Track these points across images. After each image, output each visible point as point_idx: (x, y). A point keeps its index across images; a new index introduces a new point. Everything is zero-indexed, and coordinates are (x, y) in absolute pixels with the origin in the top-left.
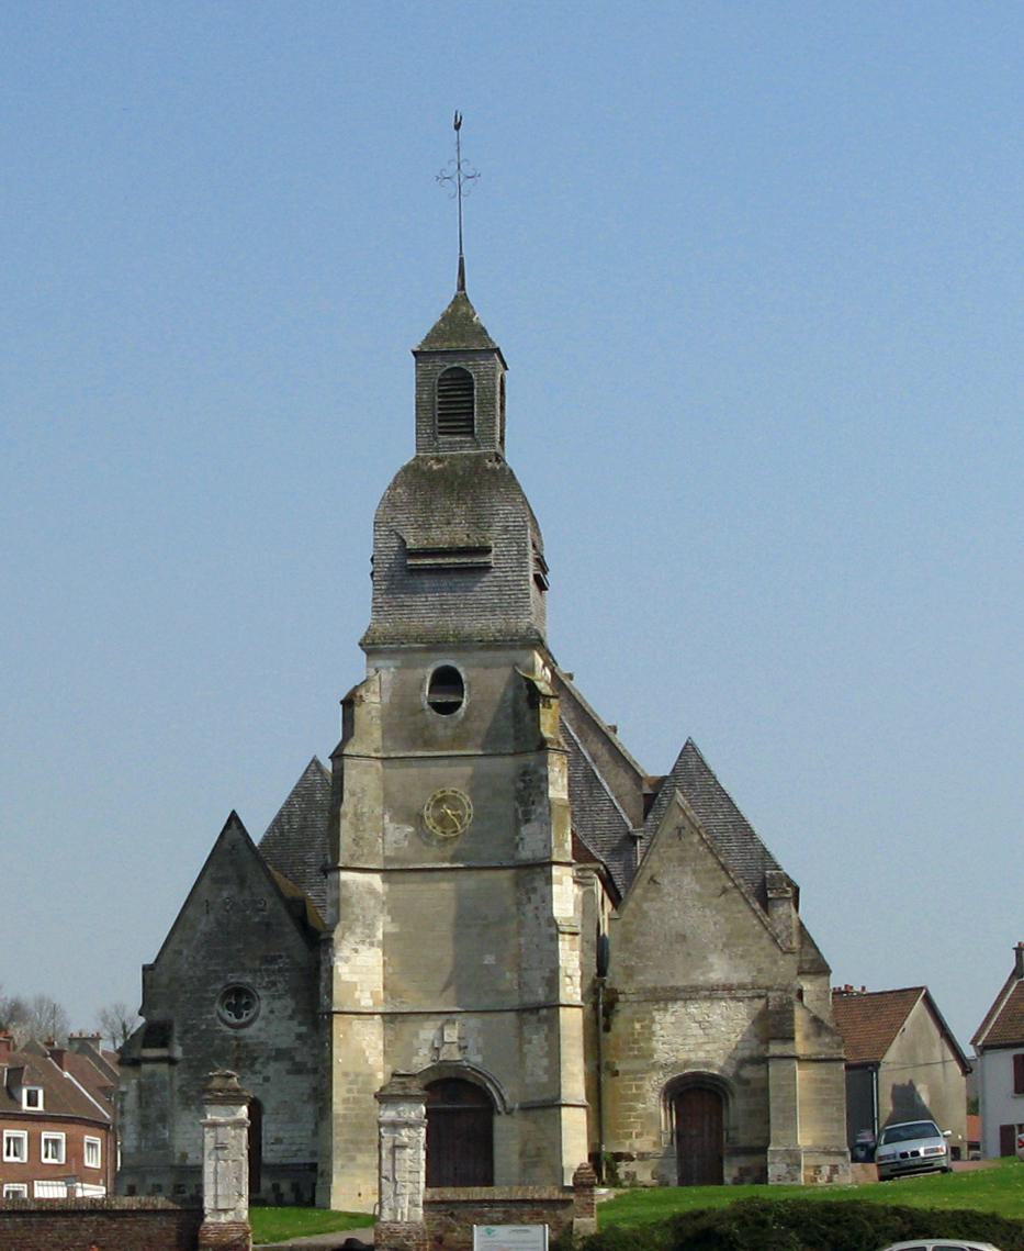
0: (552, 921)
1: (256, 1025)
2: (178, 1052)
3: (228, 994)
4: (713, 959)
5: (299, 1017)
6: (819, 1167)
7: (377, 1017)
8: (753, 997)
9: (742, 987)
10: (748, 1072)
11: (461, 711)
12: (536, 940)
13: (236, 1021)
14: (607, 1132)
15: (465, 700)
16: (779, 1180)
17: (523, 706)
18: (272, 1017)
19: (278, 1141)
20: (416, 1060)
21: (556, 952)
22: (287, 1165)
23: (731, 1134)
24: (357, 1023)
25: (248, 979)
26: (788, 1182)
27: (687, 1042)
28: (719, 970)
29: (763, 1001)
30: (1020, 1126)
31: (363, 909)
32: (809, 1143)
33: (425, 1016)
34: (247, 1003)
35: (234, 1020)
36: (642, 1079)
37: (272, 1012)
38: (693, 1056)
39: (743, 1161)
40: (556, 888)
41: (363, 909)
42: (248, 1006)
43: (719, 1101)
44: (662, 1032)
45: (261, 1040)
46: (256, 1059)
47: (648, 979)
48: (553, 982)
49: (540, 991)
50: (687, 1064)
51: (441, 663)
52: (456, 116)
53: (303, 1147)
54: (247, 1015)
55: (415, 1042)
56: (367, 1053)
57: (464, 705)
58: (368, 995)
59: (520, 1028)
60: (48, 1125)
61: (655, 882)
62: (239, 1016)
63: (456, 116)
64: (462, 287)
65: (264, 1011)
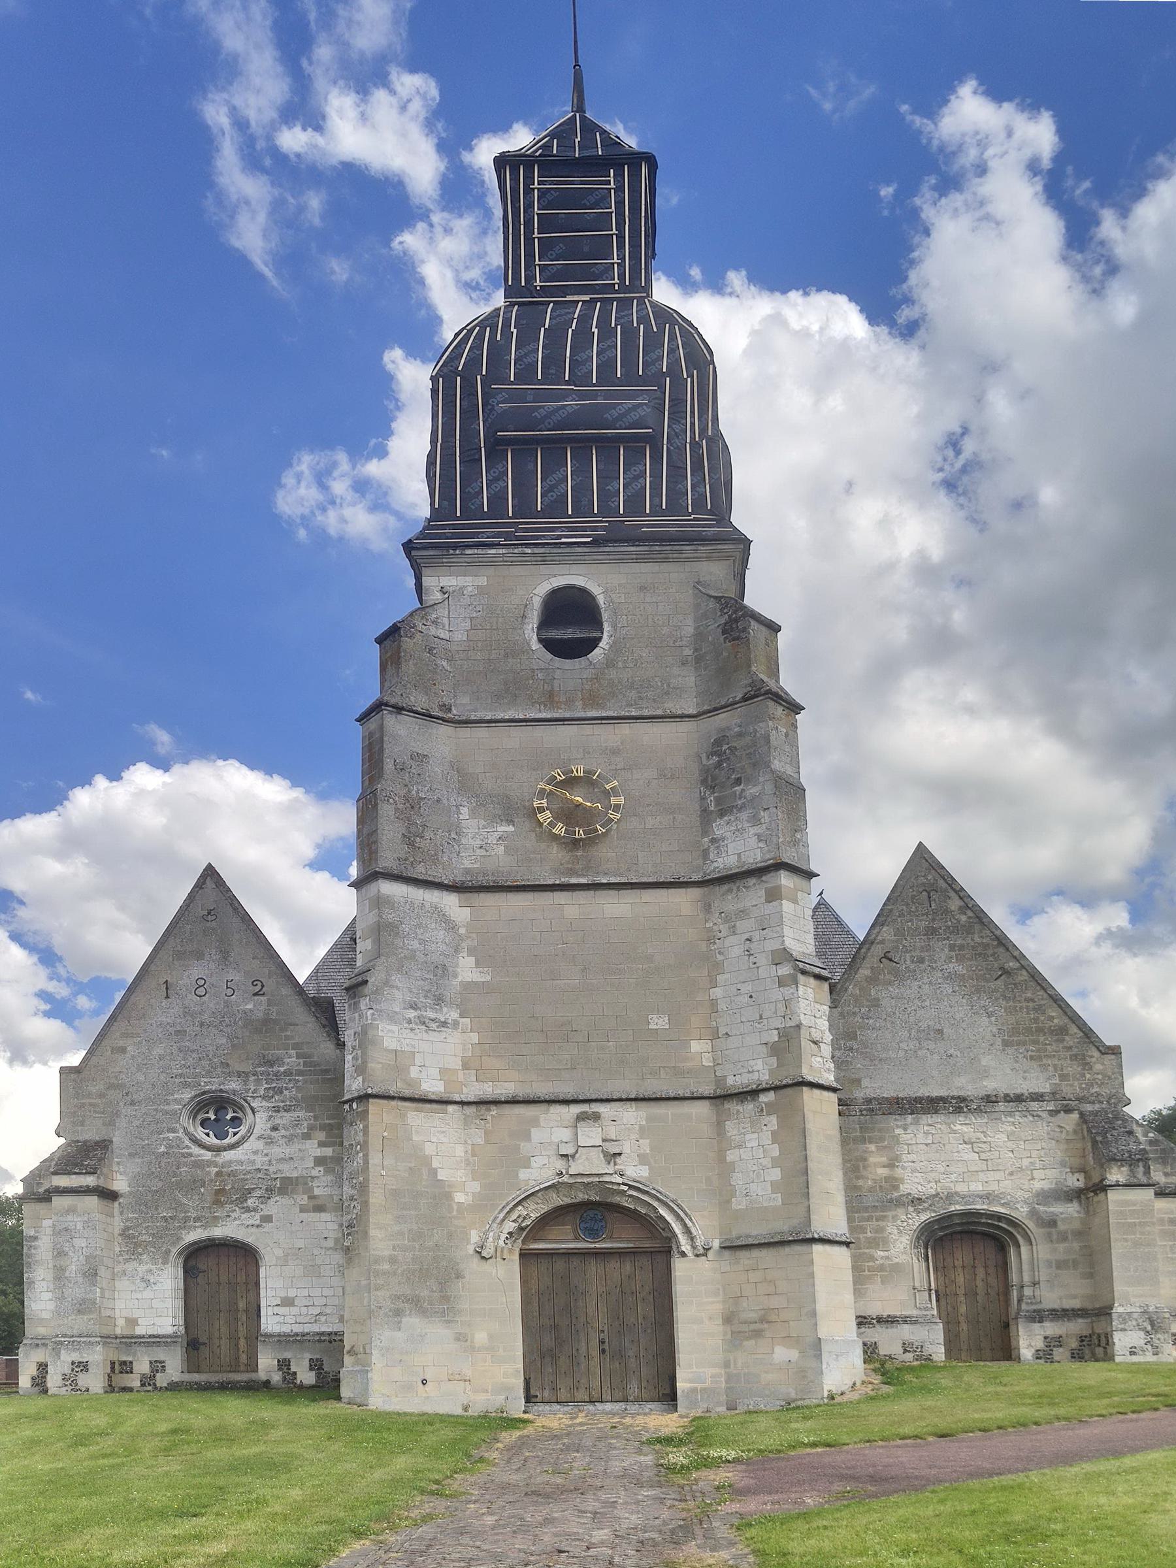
1: (252, 1144)
2: (120, 1184)
9: (1038, 1097)
11: (597, 654)
12: (747, 988)
16: (1132, 1353)
18: (274, 1134)
24: (416, 1117)
25: (233, 1085)
26: (1150, 1358)
27: (952, 1169)
31: (423, 942)
34: (233, 1119)
35: (212, 1140)
36: (883, 1218)
37: (275, 1129)
38: (961, 1188)
41: (423, 942)
42: (236, 1121)
43: (1002, 1249)
44: (912, 1157)
46: (250, 1191)
51: (580, 581)
53: (328, 1310)
54: (235, 1134)
57: (604, 643)
58: (435, 1073)
59: (720, 1126)
62: (221, 1136)
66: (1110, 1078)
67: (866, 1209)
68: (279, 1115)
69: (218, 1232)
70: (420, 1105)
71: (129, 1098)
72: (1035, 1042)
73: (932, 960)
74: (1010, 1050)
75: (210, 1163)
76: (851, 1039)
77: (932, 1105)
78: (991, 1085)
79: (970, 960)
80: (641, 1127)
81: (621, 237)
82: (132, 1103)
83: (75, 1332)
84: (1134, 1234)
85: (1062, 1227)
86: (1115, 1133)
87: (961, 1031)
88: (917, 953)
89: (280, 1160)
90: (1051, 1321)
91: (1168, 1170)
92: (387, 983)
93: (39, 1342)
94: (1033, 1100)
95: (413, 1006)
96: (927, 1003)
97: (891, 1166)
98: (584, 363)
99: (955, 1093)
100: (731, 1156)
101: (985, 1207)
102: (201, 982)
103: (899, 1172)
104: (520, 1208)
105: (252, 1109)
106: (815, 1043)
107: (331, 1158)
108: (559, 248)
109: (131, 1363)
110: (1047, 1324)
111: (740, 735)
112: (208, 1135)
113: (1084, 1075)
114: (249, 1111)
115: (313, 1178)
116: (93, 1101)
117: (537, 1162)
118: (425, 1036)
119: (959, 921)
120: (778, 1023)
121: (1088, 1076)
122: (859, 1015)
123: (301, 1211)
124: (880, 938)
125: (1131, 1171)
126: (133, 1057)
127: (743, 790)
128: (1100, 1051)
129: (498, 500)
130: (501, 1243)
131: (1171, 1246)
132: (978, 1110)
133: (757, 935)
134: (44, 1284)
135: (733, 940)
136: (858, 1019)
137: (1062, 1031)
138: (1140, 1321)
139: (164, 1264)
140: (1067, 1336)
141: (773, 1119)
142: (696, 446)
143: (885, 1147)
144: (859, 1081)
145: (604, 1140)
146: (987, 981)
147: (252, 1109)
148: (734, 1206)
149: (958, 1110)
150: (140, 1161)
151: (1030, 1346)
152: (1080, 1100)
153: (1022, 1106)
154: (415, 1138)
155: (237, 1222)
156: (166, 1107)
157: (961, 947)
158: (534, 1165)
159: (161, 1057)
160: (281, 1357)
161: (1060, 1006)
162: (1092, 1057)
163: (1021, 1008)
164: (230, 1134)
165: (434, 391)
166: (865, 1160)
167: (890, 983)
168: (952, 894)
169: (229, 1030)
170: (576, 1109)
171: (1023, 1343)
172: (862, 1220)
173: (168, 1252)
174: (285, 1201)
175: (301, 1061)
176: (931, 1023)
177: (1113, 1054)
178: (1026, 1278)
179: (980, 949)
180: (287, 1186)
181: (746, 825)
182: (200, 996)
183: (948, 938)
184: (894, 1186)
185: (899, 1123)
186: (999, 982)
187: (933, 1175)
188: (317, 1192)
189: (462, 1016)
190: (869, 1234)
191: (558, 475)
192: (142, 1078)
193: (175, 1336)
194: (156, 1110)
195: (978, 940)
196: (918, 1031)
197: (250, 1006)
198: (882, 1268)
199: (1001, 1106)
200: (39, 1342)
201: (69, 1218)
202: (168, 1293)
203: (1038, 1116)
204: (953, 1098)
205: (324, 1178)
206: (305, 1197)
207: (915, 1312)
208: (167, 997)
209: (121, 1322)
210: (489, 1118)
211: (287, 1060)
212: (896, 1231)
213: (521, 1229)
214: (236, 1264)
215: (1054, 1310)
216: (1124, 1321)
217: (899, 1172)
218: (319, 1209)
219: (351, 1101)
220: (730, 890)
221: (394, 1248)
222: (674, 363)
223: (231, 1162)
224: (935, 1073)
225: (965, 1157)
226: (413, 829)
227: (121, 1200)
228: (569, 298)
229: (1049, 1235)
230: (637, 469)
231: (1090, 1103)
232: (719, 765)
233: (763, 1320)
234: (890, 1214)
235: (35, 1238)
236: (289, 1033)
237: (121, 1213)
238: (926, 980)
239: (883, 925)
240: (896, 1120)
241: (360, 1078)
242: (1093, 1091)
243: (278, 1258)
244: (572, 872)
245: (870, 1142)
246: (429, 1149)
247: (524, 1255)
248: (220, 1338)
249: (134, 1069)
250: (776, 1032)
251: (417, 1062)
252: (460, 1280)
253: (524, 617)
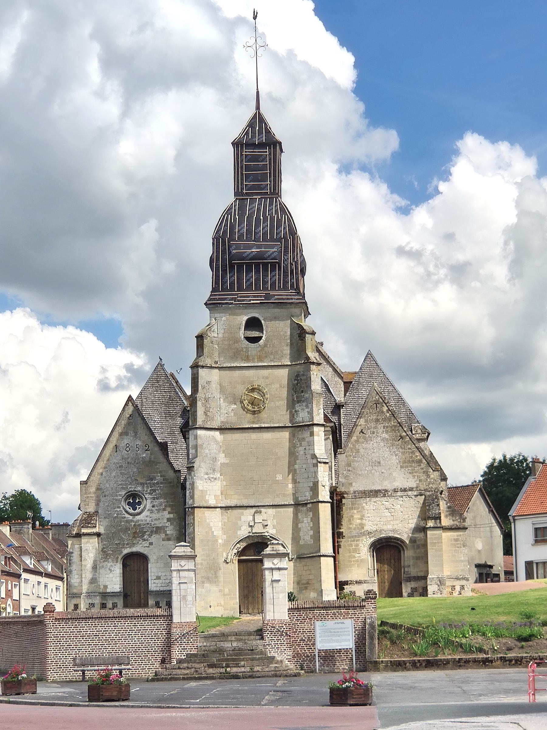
0: (314, 456)
1: (146, 513)
3: (128, 497)
5: (169, 509)
6: (454, 586)
7: (218, 509)
8: (417, 496)
9: (411, 489)
11: (261, 342)
12: (304, 466)
13: (133, 511)
15: (264, 336)
16: (434, 594)
18: (153, 509)
20: (239, 533)
21: (316, 473)
22: (164, 591)
23: (406, 570)
24: (207, 512)
25: (139, 488)
26: (439, 595)
27: (382, 520)
29: (423, 497)
30: (544, 563)
32: (449, 574)
33: (245, 508)
35: (131, 511)
37: (153, 506)
38: (385, 527)
39: (413, 584)
40: (316, 438)
41: (209, 450)
42: (140, 503)
44: (369, 515)
45: (148, 522)
46: (145, 532)
48: (315, 488)
49: (307, 494)
51: (256, 315)
52: (254, 11)
54: (139, 508)
55: (239, 522)
56: (213, 530)
57: (263, 338)
61: (363, 433)
62: (135, 509)
63: (254, 11)
64: (258, 108)
66: (436, 481)
67: (353, 537)
68: (155, 501)
69: (134, 549)
70: (209, 509)
71: (104, 494)
72: (411, 466)
73: (377, 433)
74: (403, 470)
75: (132, 521)
76: (349, 467)
77: (376, 493)
78: (398, 484)
79: (390, 432)
80: (274, 515)
81: (270, 173)
82: (105, 496)
83: (90, 592)
84: (435, 546)
85: (418, 543)
86: (433, 505)
87: (386, 462)
88: (372, 430)
89: (156, 519)
90: (414, 581)
91: (454, 519)
92: (199, 466)
93: (75, 596)
94: (410, 490)
95: (207, 474)
96: (375, 451)
97: (361, 519)
98: (258, 233)
99: (384, 488)
100: (300, 525)
101: (392, 535)
102: (128, 445)
103: (364, 521)
104: (238, 544)
105: (146, 498)
106: (324, 486)
107: (172, 518)
108: (251, 178)
109: (106, 603)
110: (412, 583)
111: (303, 375)
112: (130, 508)
113: (427, 480)
114: (144, 499)
115: (167, 527)
116: (91, 495)
117: (243, 528)
118: (210, 484)
119: (386, 416)
120: (312, 480)
121: (428, 480)
122: (352, 456)
123: (163, 540)
124: (360, 424)
125: (435, 522)
126: (105, 477)
127: (304, 395)
128: (433, 470)
129: (232, 284)
130: (232, 557)
131: (454, 550)
132: (391, 496)
133: (307, 448)
134: (76, 571)
135: (300, 448)
136: (352, 458)
137: (420, 461)
138: (436, 581)
139: (116, 563)
140: (419, 587)
141: (311, 513)
142: (291, 264)
143: (359, 511)
144: (351, 484)
145: (263, 520)
146: (396, 441)
147: (146, 498)
148: (300, 543)
149: (384, 496)
150: (108, 520)
151: (406, 591)
152: (426, 490)
153: (406, 493)
154: (207, 521)
155: (141, 545)
156: (116, 498)
157: (387, 427)
158: (242, 529)
159: (115, 477)
160: (156, 601)
161: (419, 451)
162: (430, 472)
163: (407, 452)
164: (138, 508)
165: (213, 244)
166: (353, 517)
167: (363, 443)
168: (384, 405)
169: (137, 465)
170: (254, 510)
171: (404, 591)
172: (351, 541)
173: (118, 558)
174: (157, 536)
175: (162, 478)
176: (377, 459)
177: (437, 471)
178: (406, 564)
179: (393, 428)
180: (158, 530)
181: (305, 408)
182: (127, 451)
183: (382, 423)
184: (362, 527)
185: (364, 501)
186: (400, 441)
187: (375, 522)
188: (168, 532)
189: (221, 475)
190: (354, 547)
191: (250, 275)
192: (108, 486)
193: (120, 592)
194: (113, 499)
195: (393, 424)
196: (372, 463)
197: (144, 455)
198: (357, 561)
199: (399, 494)
200: (75, 596)
201: (88, 545)
202: (118, 575)
203: (411, 497)
204: (383, 490)
205: (170, 527)
206: (164, 534)
207: (368, 579)
208: (116, 452)
209: (102, 587)
210: (229, 512)
211: (157, 478)
212: (363, 546)
213: (238, 552)
214: (140, 562)
215: (415, 577)
216: (431, 581)
217: (364, 521)
218: (169, 539)
219: (189, 508)
220: (300, 430)
221: (202, 559)
222: (285, 233)
223: (139, 520)
224: (377, 480)
225: (386, 514)
226: (207, 409)
227: (102, 536)
228: (254, 197)
229: (414, 546)
230: (274, 273)
231: (428, 491)
232: (297, 384)
233: (308, 583)
234: (361, 539)
235: (72, 553)
236: (158, 467)
237: (102, 542)
238: (375, 441)
239: (361, 418)
240: (363, 500)
241: (192, 500)
242: (430, 486)
243: (155, 560)
244: (253, 423)
245: (355, 509)
246: (212, 524)
247: (239, 561)
248: (135, 593)
249: (105, 481)
250: (312, 483)
251: (208, 494)
252: (220, 571)
253: (240, 328)
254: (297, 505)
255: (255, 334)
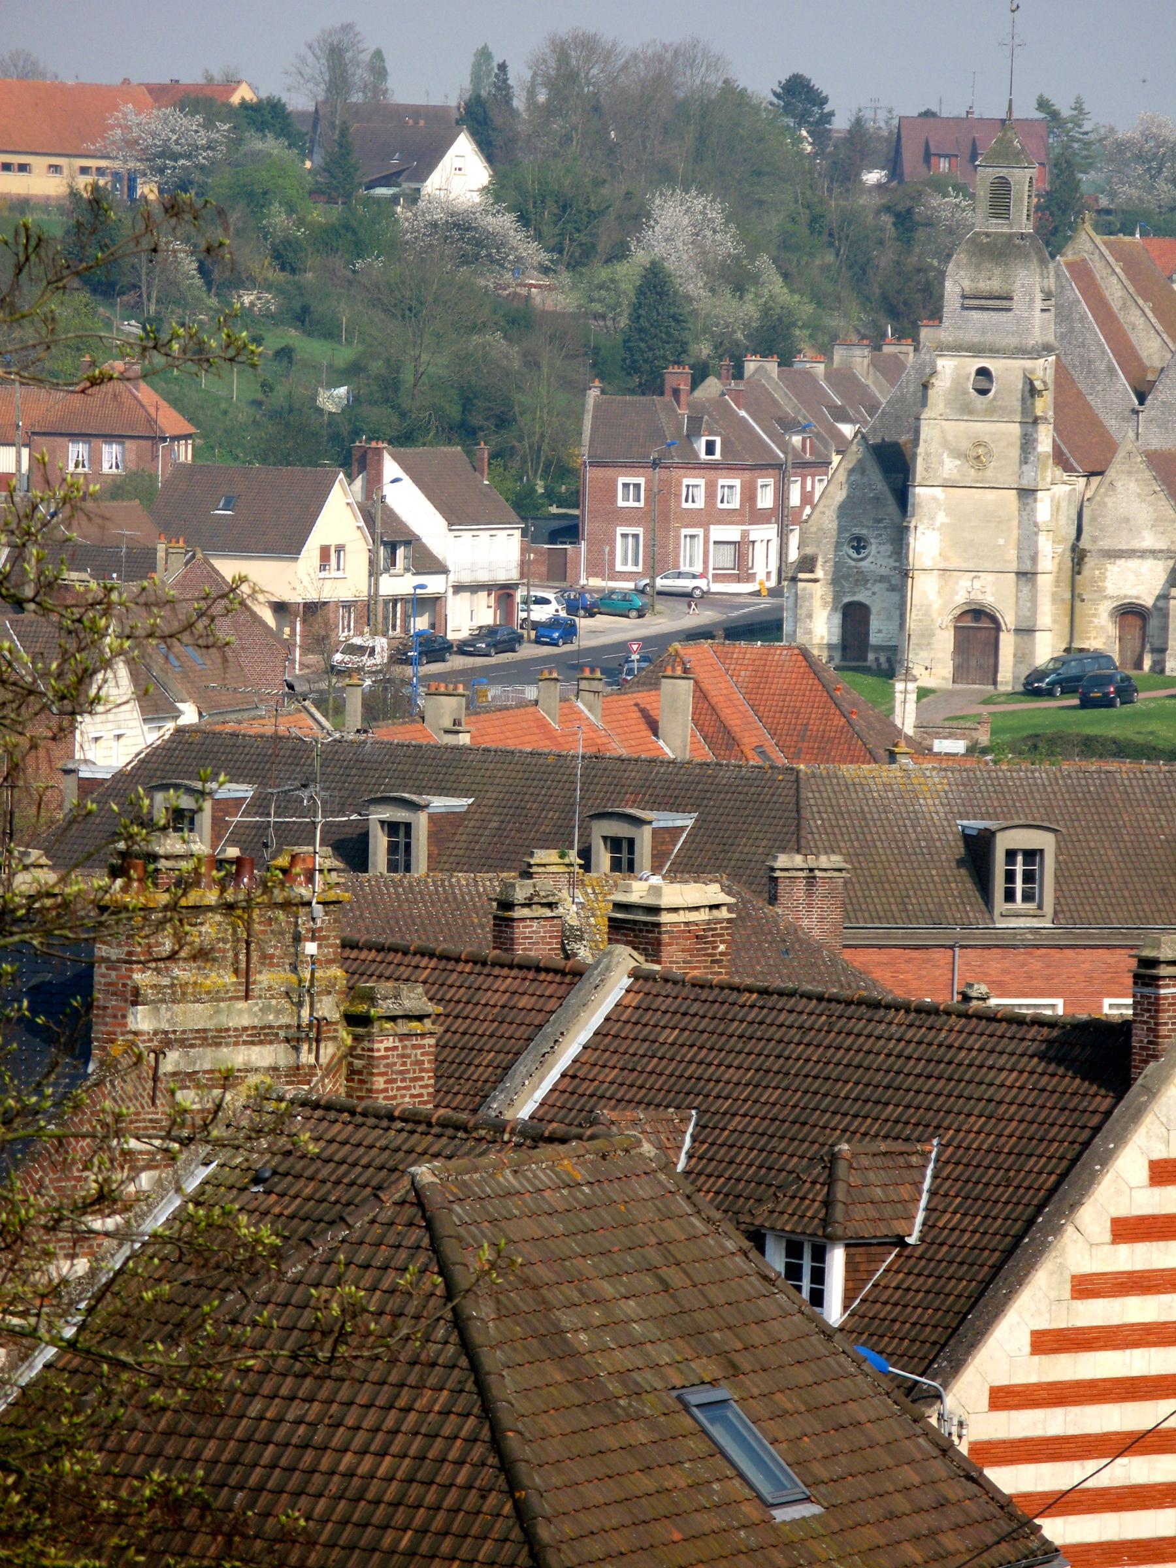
0: (1036, 525)
1: (870, 559)
3: (852, 540)
4: (1145, 534)
9: (1161, 551)
10: (1161, 604)
11: (991, 394)
14: (1076, 635)
17: (1027, 394)
19: (880, 631)
25: (864, 532)
28: (1149, 540)
35: (855, 556)
42: (864, 547)
47: (1105, 544)
50: (1125, 597)
60: (724, 472)
65: (873, 552)
69: (855, 598)
247: (956, 628)
254: (1020, 574)
255: (984, 385)
